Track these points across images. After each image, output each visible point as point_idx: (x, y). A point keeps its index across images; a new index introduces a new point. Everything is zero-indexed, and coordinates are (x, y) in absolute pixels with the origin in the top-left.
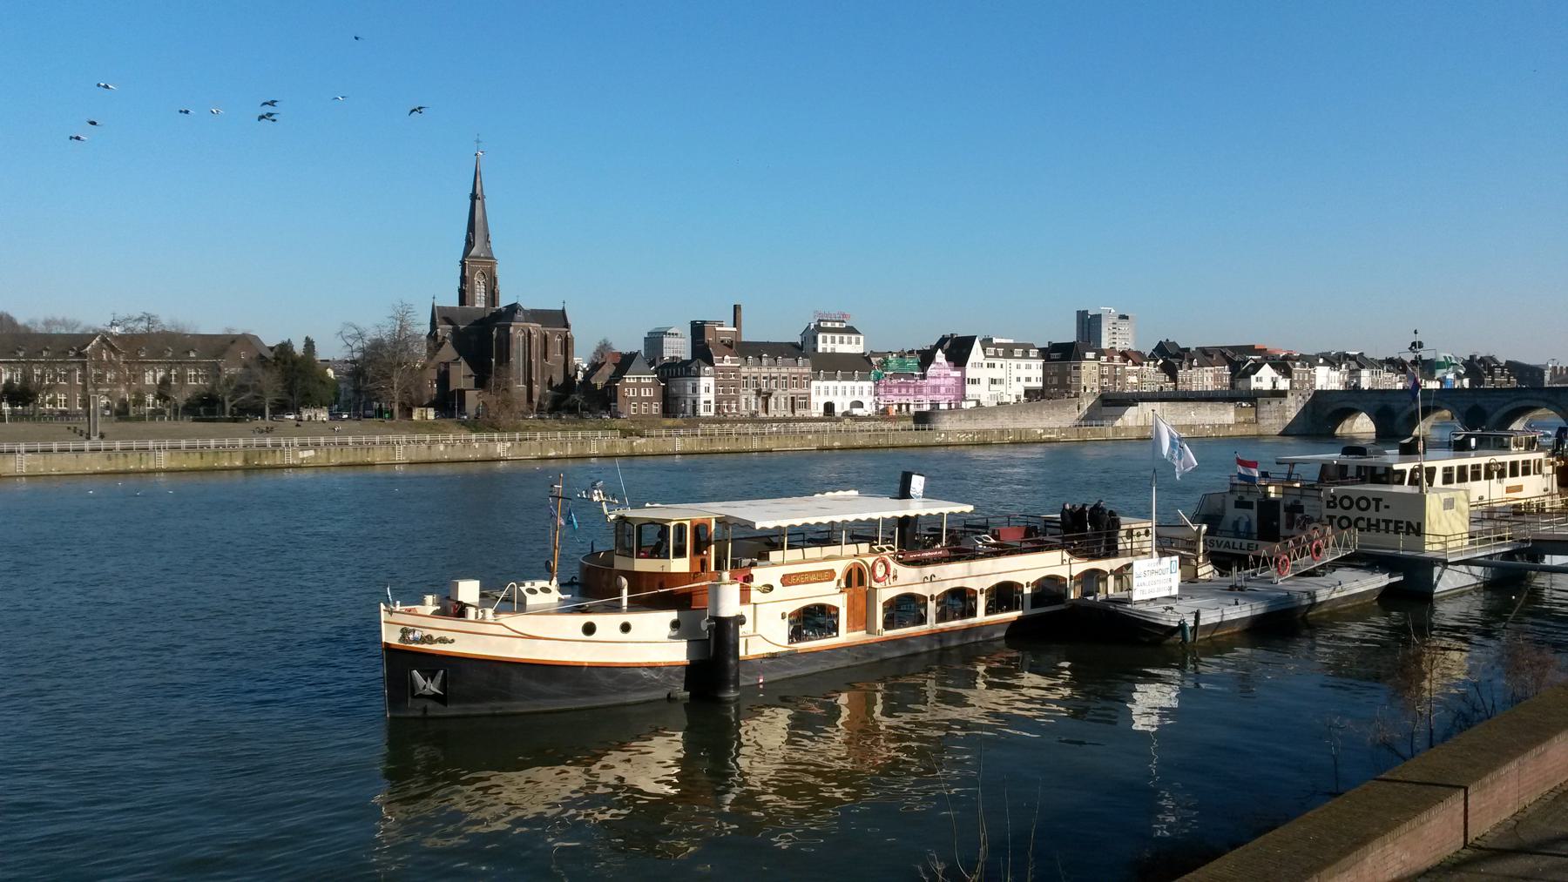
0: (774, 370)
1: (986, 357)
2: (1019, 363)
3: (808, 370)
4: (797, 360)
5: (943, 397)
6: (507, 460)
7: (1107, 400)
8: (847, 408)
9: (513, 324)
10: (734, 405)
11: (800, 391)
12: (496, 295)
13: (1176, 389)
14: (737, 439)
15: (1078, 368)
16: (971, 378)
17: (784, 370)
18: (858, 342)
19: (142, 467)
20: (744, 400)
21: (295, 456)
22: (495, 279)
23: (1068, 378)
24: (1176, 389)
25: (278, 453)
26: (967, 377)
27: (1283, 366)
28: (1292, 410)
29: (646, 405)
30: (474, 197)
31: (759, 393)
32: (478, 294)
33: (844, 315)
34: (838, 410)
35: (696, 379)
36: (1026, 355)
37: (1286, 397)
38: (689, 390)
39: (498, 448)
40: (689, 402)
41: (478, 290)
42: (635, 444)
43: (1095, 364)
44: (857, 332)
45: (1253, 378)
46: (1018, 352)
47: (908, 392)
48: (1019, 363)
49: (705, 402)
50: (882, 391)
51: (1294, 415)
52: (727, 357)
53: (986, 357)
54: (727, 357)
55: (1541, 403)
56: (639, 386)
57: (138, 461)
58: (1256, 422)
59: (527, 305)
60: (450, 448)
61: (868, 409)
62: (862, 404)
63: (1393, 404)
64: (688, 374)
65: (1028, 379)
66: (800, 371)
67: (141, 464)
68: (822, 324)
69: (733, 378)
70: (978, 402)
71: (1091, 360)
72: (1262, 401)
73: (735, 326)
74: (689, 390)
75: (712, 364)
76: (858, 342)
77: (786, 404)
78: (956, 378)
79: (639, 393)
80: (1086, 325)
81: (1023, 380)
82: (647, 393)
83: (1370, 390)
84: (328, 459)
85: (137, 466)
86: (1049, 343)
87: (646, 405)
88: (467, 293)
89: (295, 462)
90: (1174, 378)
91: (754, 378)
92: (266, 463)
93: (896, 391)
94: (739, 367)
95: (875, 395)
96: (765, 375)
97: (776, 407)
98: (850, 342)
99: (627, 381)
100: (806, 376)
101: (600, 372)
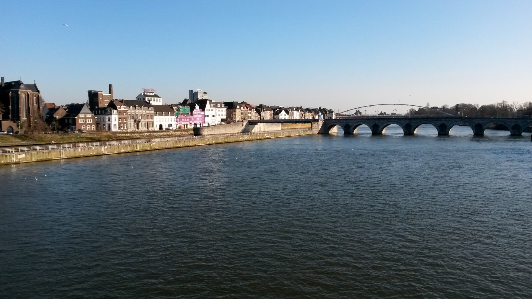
0: (141, 112)
1: (211, 107)
3: (153, 112)
4: (149, 108)
6: (106, 155)
7: (251, 123)
8: (167, 127)
9: (20, 90)
10: (125, 126)
11: (150, 120)
13: (260, 118)
14: (185, 141)
15: (235, 111)
17: (144, 112)
20: (129, 124)
23: (231, 115)
24: (260, 118)
25: (8, 157)
26: (205, 114)
27: (287, 111)
29: (89, 127)
31: (135, 121)
33: (153, 90)
34: (164, 128)
36: (221, 107)
38: (107, 120)
39: (102, 149)
40: (107, 125)
42: (152, 145)
43: (240, 110)
44: (159, 97)
45: (280, 114)
46: (219, 105)
47: (187, 120)
49: (114, 125)
50: (178, 120)
52: (122, 106)
53: (211, 107)
54: (122, 106)
55: (391, 122)
56: (86, 118)
58: (312, 130)
60: (83, 150)
61: (174, 127)
64: (106, 113)
65: (222, 115)
66: (150, 112)
69: (125, 115)
70: (209, 124)
73: (110, 93)
74: (107, 120)
75: (116, 109)
76: (160, 101)
77: (145, 125)
78: (202, 115)
79: (86, 121)
80: (192, 95)
81: (220, 115)
82: (89, 121)
84: (31, 158)
87: (89, 127)
89: (16, 161)
90: (260, 115)
92: (3, 162)
93: (183, 120)
95: (176, 121)
97: (142, 126)
98: (157, 101)
99: (80, 116)
101: (57, 112)
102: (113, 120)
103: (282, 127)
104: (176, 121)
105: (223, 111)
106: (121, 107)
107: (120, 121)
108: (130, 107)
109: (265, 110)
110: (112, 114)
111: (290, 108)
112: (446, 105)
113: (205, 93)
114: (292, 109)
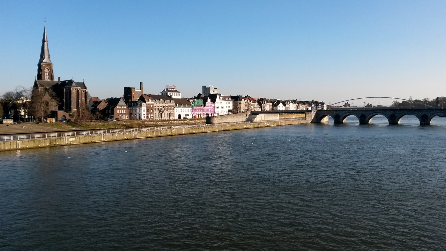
0: (164, 104)
1: (220, 100)
2: (227, 102)
3: (174, 104)
4: (170, 101)
5: (210, 112)
6: (137, 139)
8: (184, 116)
9: (72, 87)
10: (152, 116)
11: (171, 111)
12: (53, 77)
13: (261, 110)
14: (199, 128)
15: (240, 103)
16: (216, 106)
17: (167, 104)
18: (179, 95)
19: (11, 148)
20: (155, 114)
21: (68, 140)
22: (52, 71)
23: (237, 107)
24: (261, 110)
26: (216, 106)
27: (284, 104)
28: (313, 116)
29: (124, 116)
30: (44, 41)
31: (160, 111)
32: (46, 76)
33: (174, 87)
34: (182, 117)
35: (140, 107)
36: (228, 100)
37: (312, 112)
38: (138, 111)
39: (134, 134)
40: (138, 115)
41: (46, 75)
42: (172, 131)
44: (179, 92)
45: (278, 106)
48: (227, 102)
49: (143, 115)
50: (194, 110)
51: (313, 117)
52: (150, 100)
53: (220, 100)
54: (150, 100)
55: (377, 113)
56: (122, 109)
57: (9, 145)
58: (305, 119)
59: (76, 80)
61: (190, 117)
62: (188, 115)
63: (339, 114)
64: (137, 105)
65: (229, 107)
66: (171, 104)
67: (11, 146)
68: (168, 89)
69: (152, 107)
70: (218, 114)
71: (243, 101)
72: (307, 113)
73: (141, 89)
74: (138, 111)
75: (145, 102)
76: (179, 95)
77: (167, 115)
78: (213, 106)
80: (205, 90)
83: (326, 110)
84: (80, 141)
85: (9, 148)
86: (194, 97)
87: (124, 116)
88: (42, 76)
89: (68, 143)
90: (261, 106)
91: (158, 107)
93: (197, 110)
94: (153, 103)
95: (192, 112)
96: (167, 106)
97: (164, 116)
99: (117, 108)
100: (173, 106)
101: (100, 104)
102: (142, 111)
103: (279, 117)
104: (192, 112)
105: (230, 103)
106: (149, 100)
107: (148, 112)
108: (156, 100)
109: (265, 102)
110: (141, 106)
111: (286, 101)
112: (428, 98)
113: (215, 88)
114: (288, 101)
